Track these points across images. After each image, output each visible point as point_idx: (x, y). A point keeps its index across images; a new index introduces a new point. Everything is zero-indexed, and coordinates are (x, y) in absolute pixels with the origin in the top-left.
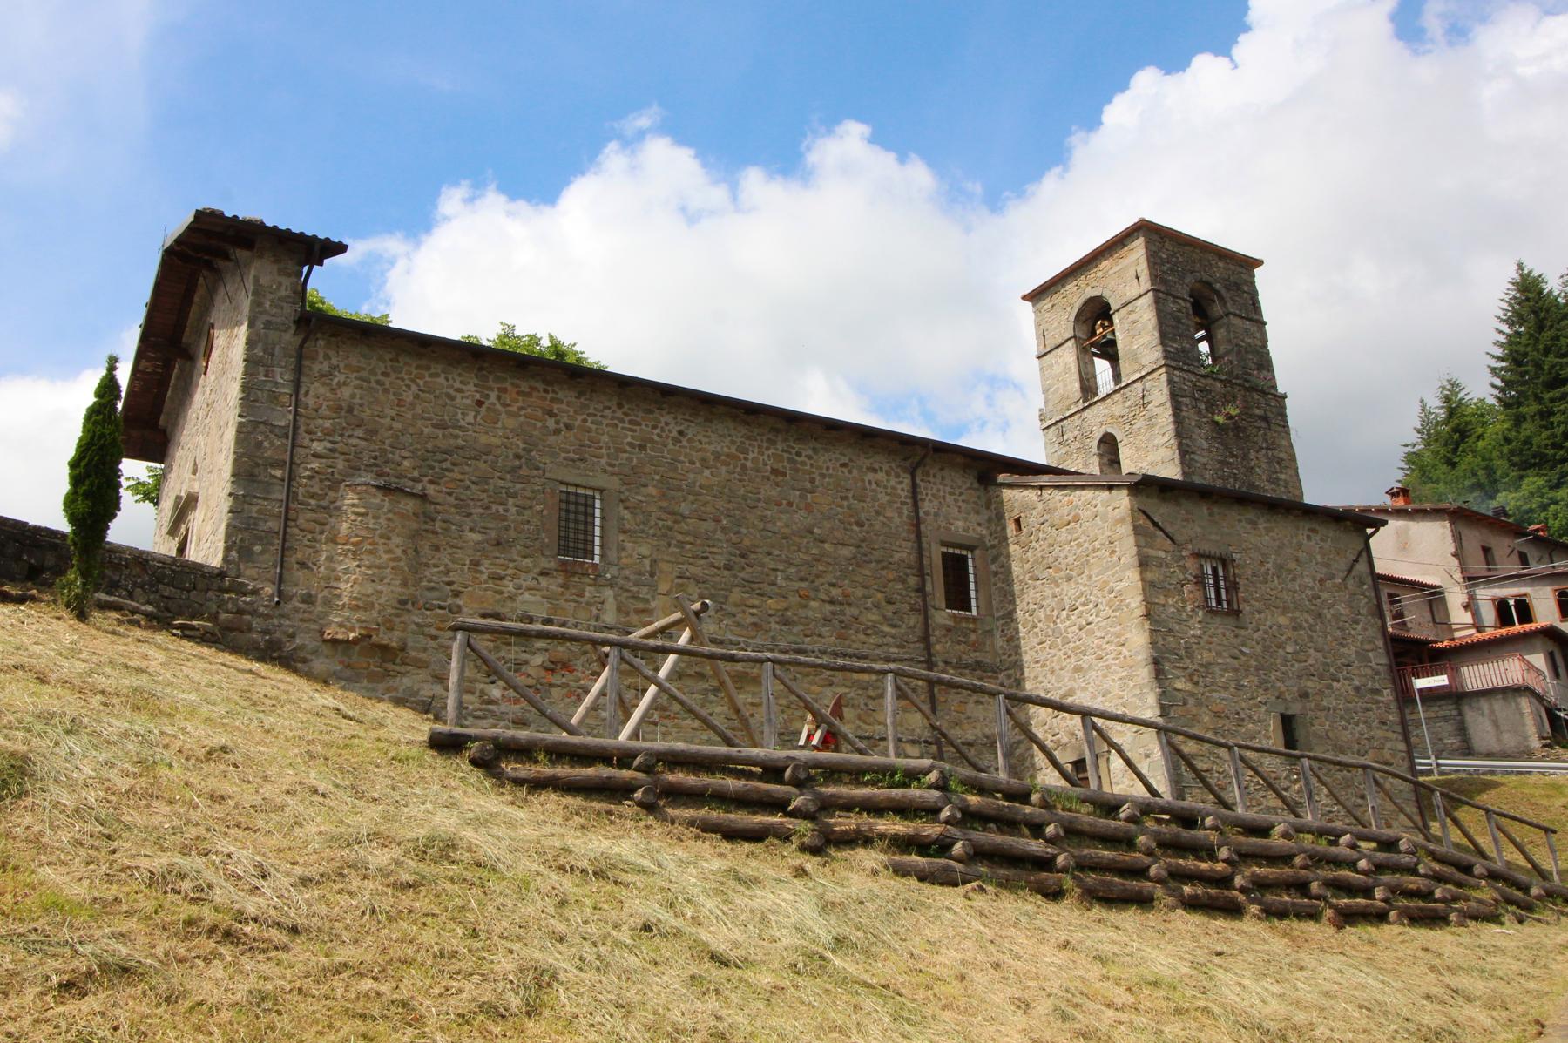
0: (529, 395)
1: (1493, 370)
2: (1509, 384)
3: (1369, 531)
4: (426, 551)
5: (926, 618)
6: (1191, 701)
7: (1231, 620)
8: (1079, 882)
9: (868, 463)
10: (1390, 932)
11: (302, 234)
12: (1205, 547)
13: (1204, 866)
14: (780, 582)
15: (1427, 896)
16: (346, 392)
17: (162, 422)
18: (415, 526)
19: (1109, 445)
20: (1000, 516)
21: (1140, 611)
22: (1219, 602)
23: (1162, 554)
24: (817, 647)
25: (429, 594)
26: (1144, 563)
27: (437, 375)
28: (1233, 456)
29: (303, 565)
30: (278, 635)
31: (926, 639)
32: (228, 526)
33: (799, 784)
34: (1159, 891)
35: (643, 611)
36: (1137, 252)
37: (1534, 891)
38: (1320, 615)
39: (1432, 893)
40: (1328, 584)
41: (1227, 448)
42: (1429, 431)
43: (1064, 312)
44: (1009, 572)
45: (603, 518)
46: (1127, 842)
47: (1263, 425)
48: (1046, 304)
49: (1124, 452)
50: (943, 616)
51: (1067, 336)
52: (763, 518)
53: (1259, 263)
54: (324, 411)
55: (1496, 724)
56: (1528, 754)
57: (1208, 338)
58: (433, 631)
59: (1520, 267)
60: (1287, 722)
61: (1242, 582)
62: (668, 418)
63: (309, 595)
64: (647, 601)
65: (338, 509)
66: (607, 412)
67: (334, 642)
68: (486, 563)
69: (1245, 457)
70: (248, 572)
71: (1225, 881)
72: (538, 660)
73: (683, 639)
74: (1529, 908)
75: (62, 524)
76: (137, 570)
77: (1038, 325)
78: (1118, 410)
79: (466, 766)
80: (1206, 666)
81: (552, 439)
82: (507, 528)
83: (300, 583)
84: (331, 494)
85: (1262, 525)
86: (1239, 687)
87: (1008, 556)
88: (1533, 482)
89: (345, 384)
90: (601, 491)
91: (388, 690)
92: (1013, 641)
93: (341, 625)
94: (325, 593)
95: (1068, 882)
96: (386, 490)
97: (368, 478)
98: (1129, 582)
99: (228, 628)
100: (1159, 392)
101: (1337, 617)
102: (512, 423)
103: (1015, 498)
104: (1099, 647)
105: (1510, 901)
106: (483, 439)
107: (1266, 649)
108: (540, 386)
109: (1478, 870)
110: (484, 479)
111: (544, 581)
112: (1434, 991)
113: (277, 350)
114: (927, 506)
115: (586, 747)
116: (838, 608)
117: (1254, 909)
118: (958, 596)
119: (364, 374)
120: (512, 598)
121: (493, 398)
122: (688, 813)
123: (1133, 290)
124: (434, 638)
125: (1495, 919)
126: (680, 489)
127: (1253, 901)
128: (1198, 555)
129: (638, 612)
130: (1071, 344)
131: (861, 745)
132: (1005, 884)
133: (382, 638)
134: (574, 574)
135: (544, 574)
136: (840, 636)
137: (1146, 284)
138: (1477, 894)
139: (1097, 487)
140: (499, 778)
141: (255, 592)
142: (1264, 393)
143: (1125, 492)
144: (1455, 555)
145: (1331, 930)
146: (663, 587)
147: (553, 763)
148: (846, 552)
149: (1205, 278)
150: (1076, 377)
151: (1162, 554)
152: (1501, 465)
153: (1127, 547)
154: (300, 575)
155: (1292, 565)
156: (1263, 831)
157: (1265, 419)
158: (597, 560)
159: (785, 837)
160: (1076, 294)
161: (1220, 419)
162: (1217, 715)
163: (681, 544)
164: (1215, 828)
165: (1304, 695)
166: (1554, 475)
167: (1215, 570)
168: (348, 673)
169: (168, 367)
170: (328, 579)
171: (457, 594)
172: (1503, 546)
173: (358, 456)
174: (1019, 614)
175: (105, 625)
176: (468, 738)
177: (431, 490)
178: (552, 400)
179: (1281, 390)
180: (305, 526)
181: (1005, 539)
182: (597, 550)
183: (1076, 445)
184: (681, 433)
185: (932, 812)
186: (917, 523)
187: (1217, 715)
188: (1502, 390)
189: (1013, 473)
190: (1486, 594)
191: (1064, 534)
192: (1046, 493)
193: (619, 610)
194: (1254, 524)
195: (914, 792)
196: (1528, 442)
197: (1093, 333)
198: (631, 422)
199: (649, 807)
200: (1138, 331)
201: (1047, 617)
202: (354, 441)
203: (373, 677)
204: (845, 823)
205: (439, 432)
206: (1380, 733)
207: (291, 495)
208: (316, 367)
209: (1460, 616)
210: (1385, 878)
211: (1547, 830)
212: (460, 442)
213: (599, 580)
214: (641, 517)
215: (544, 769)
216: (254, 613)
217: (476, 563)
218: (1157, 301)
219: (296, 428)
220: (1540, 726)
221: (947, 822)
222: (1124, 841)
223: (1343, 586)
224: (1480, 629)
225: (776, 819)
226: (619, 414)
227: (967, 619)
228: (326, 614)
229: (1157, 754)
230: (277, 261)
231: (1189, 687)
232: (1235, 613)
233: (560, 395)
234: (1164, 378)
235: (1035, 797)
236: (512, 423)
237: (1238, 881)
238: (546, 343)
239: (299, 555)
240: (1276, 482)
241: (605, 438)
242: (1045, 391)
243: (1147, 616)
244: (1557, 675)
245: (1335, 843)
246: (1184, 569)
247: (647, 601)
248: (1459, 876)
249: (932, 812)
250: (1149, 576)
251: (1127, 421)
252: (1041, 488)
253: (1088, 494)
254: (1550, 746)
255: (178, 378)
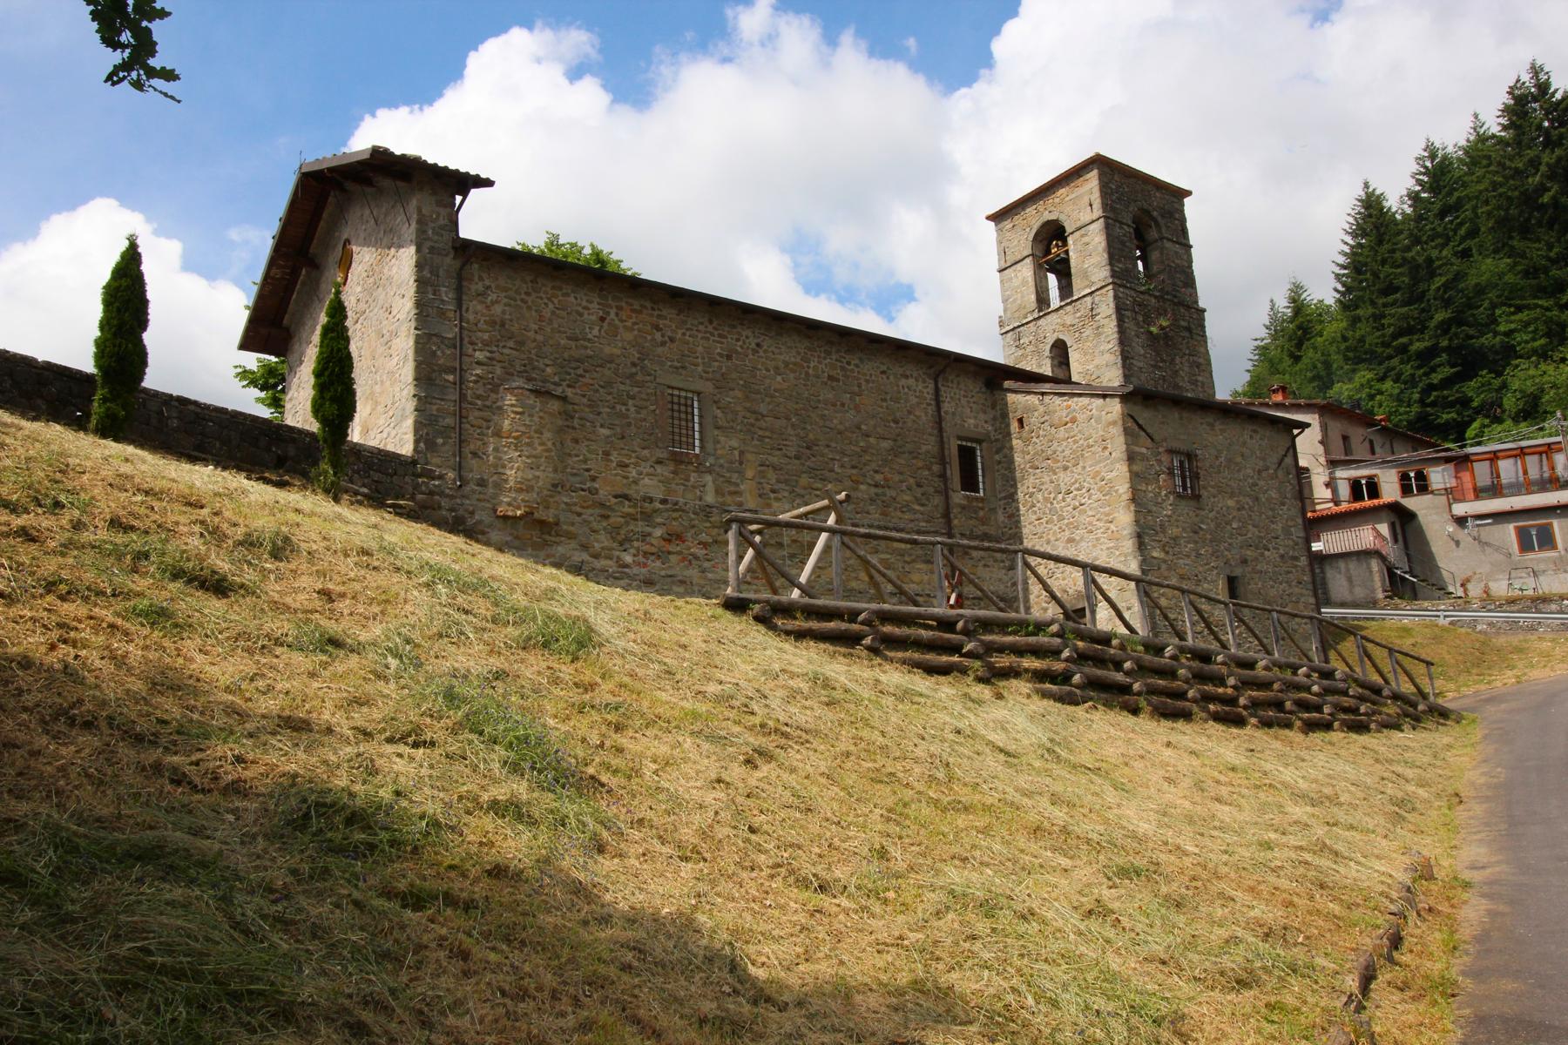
0: (640, 312)
1: (1338, 277)
2: (1349, 289)
3: (1296, 432)
4: (569, 443)
5: (947, 498)
6: (1164, 566)
7: (1192, 503)
8: (1150, 704)
9: (901, 371)
10: (1336, 736)
11: (457, 171)
12: (1175, 445)
13: (1221, 690)
14: (837, 469)
15: (1355, 711)
16: (498, 309)
17: (285, 322)
18: (560, 422)
19: (1060, 351)
20: (1004, 415)
21: (1126, 496)
22: (1185, 489)
23: (1144, 450)
24: (866, 522)
25: (572, 479)
26: (1131, 458)
27: (567, 295)
28: (1163, 361)
29: (475, 454)
30: (461, 512)
31: (947, 515)
32: (416, 422)
33: (966, 632)
34: (1195, 709)
35: (735, 493)
36: (1091, 184)
37: (1421, 707)
38: (1257, 499)
39: (1358, 709)
40: (1264, 474)
41: (1158, 354)
42: (1277, 328)
43: (1022, 236)
44: (1012, 461)
45: (701, 417)
46: (1170, 674)
47: (1187, 334)
48: (1007, 224)
49: (1074, 356)
50: (959, 497)
51: (1026, 253)
52: (823, 417)
53: (1188, 193)
54: (482, 325)
55: (1350, 580)
56: (1373, 604)
57: (1143, 258)
58: (578, 509)
59: (1366, 185)
60: (1232, 583)
61: (1202, 473)
62: (748, 332)
63: (482, 479)
64: (737, 485)
65: (500, 408)
66: (701, 328)
67: (505, 518)
68: (615, 453)
69: (1172, 361)
70: (434, 460)
71: (1232, 701)
72: (658, 532)
73: (831, 520)
74: (1418, 720)
75: (314, 426)
76: (352, 459)
77: (1000, 242)
78: (1069, 320)
79: (751, 621)
80: (1175, 539)
81: (660, 350)
82: (629, 424)
83: (475, 469)
84: (493, 396)
85: (1218, 426)
86: (1198, 555)
87: (1011, 448)
88: (1364, 375)
89: (497, 302)
90: (699, 394)
91: (548, 556)
92: (1014, 518)
93: (509, 504)
94: (495, 478)
95: (1143, 703)
96: (537, 392)
97: (519, 382)
98: (1118, 473)
99: (423, 506)
100: (1106, 306)
101: (1269, 500)
102: (629, 336)
103: (1018, 401)
104: (1090, 523)
105: (1407, 715)
106: (607, 350)
107: (1218, 526)
108: (648, 304)
109: (1386, 692)
110: (609, 384)
111: (659, 469)
112: (1386, 775)
113: (441, 273)
114: (947, 407)
115: (825, 607)
116: (879, 491)
117: (1253, 720)
118: (969, 483)
119: (511, 293)
120: (635, 482)
121: (612, 315)
122: (900, 655)
123: (1086, 216)
124: (579, 515)
125: (1398, 727)
126: (758, 392)
127: (1252, 715)
128: (1170, 451)
129: (731, 493)
130: (1028, 260)
131: (1002, 605)
132: (1108, 705)
133: (540, 514)
134: (682, 462)
135: (659, 462)
136: (884, 514)
137: (1098, 211)
138: (1385, 710)
139: (1093, 396)
140: (772, 627)
141: (441, 477)
142: (1188, 307)
143: (1117, 400)
144: (1321, 442)
145: (1302, 736)
146: (750, 474)
147: (807, 618)
148: (886, 444)
149: (1146, 206)
150: (1033, 289)
151: (1144, 450)
152: (1337, 361)
153: (1118, 445)
154: (474, 462)
155: (1239, 459)
156: (1251, 665)
157: (1188, 329)
158: (697, 451)
159: (964, 671)
160: (1035, 218)
161: (1154, 329)
162: (1182, 577)
163: (761, 438)
164: (1223, 663)
165: (1244, 561)
166: (1382, 370)
167: (1181, 463)
168: (517, 543)
169: (295, 273)
170: (496, 466)
171: (593, 479)
172: (1358, 434)
173: (511, 363)
174: (1020, 495)
175: (181, 487)
176: (750, 601)
177: (569, 392)
178: (659, 316)
179: (1201, 304)
180: (475, 422)
181: (1009, 434)
182: (697, 443)
183: (1031, 348)
184: (758, 345)
185: (1056, 653)
186: (939, 421)
187: (1182, 577)
188: (1343, 294)
189: (1017, 380)
190: (1343, 474)
191: (1062, 432)
192: (1047, 398)
193: (717, 492)
194: (1212, 426)
195: (1042, 639)
196: (1362, 340)
197: (1048, 252)
198: (720, 336)
199: (874, 650)
200: (1089, 253)
201: (1046, 499)
202: (506, 351)
203: (536, 547)
204: (1002, 661)
205: (573, 344)
206: (1297, 590)
207: (462, 397)
208: (473, 287)
209: (1321, 492)
210: (1329, 698)
211: (1429, 664)
212: (589, 352)
213: (701, 469)
214: (730, 416)
215: (801, 623)
216: (442, 494)
217: (607, 454)
218: (1107, 227)
219: (462, 339)
220: (1383, 581)
221: (1067, 660)
222: (1170, 674)
223: (1274, 477)
224: (1337, 503)
225: (956, 659)
226: (710, 328)
227: (977, 499)
228: (495, 496)
229: (1137, 607)
230: (434, 193)
231: (1162, 555)
232: (1196, 497)
233: (664, 313)
234: (1111, 293)
235: (1115, 642)
236: (629, 336)
237: (1242, 701)
238: (587, 251)
239: (472, 447)
240: (1195, 383)
241: (700, 349)
242: (1005, 301)
243: (1133, 500)
244: (1396, 541)
245: (1295, 673)
246: (1159, 461)
247: (737, 485)
248: (1374, 697)
249: (1056, 653)
250: (1136, 468)
251: (1077, 330)
252: (1043, 394)
253: (1085, 400)
254: (1391, 598)
255: (304, 284)
